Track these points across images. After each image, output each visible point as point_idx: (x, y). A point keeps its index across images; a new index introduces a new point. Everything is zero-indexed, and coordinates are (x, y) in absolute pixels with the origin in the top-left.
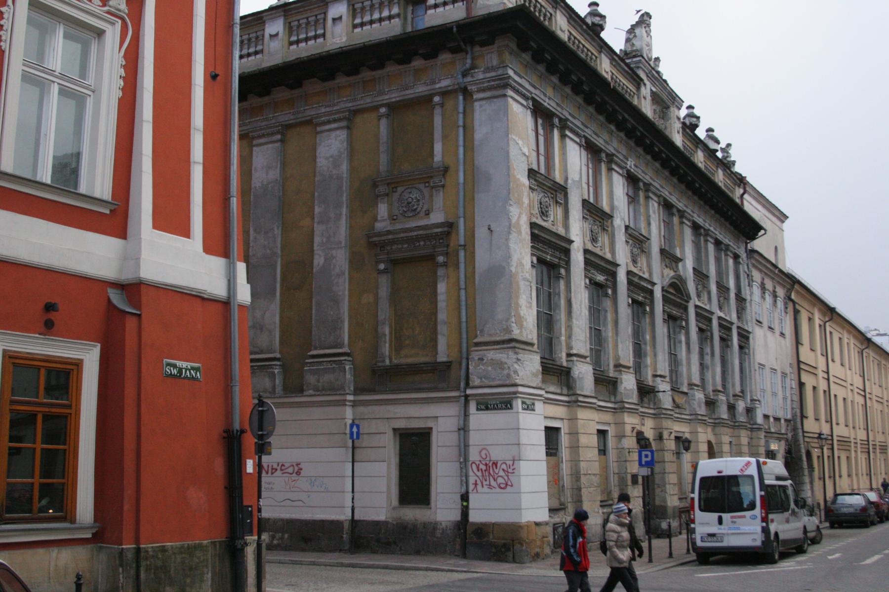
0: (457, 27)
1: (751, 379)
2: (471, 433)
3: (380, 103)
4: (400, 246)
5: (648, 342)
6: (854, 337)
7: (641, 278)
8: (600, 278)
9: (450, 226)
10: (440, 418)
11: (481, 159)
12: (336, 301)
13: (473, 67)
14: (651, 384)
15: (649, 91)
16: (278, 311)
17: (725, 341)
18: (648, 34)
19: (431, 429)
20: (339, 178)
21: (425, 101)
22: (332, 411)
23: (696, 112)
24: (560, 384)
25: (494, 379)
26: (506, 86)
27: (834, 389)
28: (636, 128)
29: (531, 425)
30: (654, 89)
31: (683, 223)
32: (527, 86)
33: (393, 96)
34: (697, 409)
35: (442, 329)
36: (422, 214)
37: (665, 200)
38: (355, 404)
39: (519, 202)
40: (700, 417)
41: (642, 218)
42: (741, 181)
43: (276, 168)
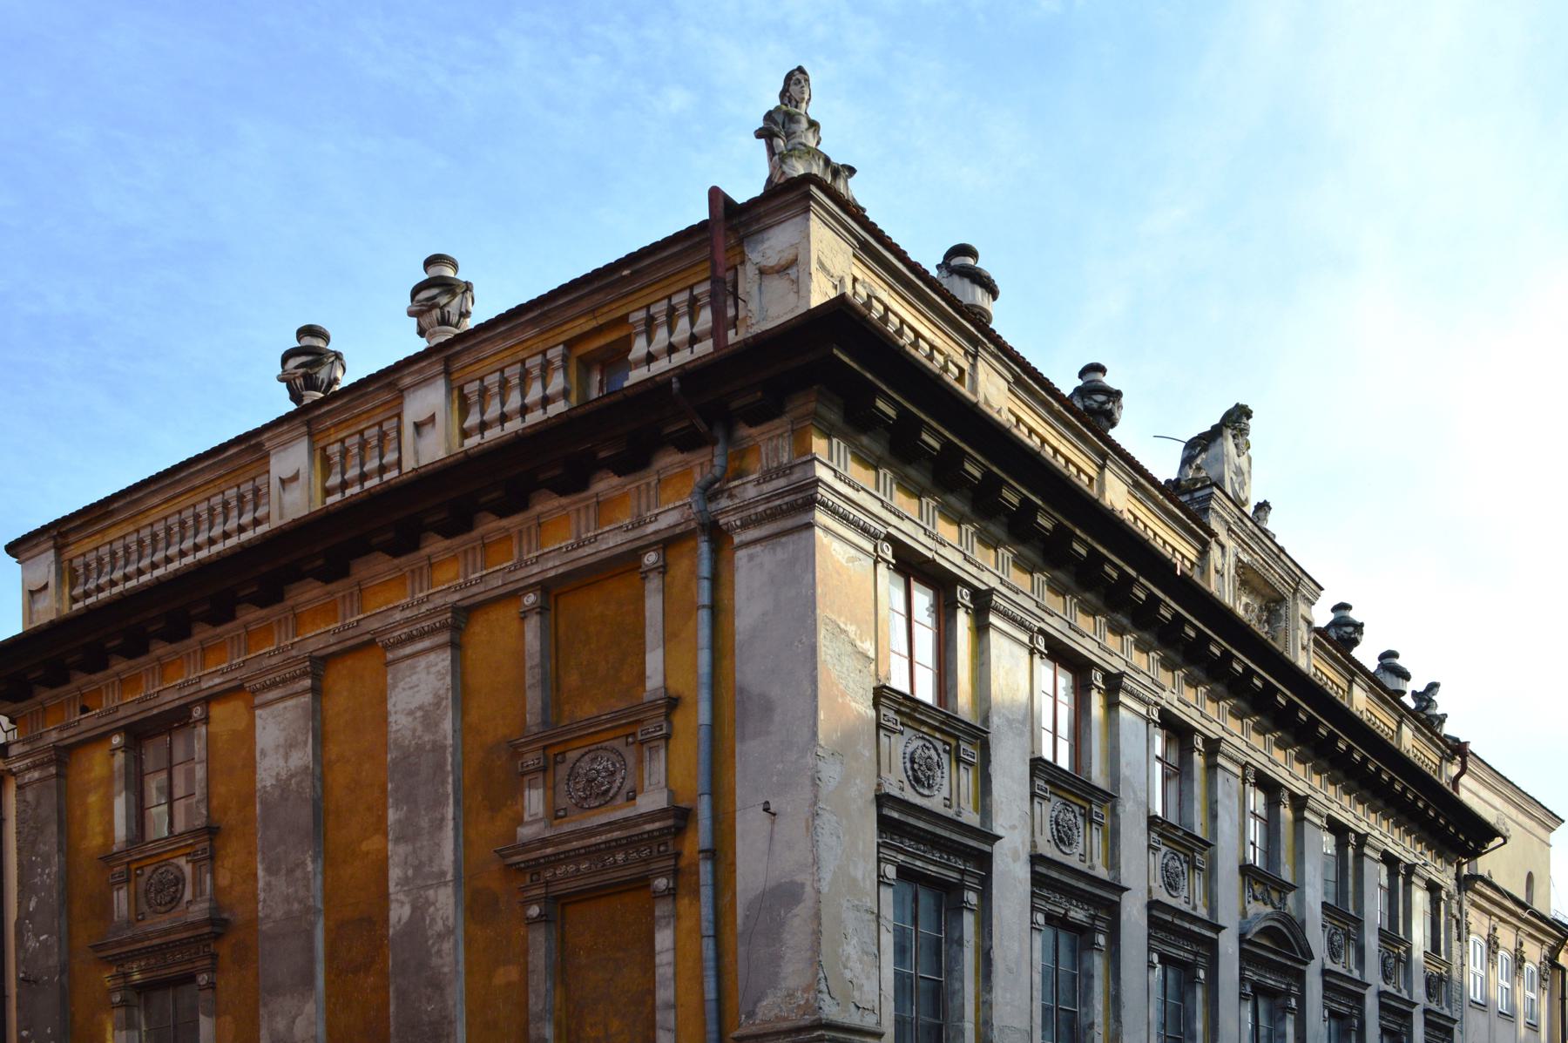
3: (521, 584)
4: (572, 868)
8: (1078, 915)
9: (681, 816)
11: (749, 671)
12: (437, 985)
15: (1232, 560)
18: (1243, 448)
20: (438, 748)
21: (625, 564)
23: (1354, 615)
28: (1133, 581)
30: (1245, 558)
32: (875, 507)
33: (550, 565)
36: (620, 800)
42: (1457, 750)
43: (306, 743)
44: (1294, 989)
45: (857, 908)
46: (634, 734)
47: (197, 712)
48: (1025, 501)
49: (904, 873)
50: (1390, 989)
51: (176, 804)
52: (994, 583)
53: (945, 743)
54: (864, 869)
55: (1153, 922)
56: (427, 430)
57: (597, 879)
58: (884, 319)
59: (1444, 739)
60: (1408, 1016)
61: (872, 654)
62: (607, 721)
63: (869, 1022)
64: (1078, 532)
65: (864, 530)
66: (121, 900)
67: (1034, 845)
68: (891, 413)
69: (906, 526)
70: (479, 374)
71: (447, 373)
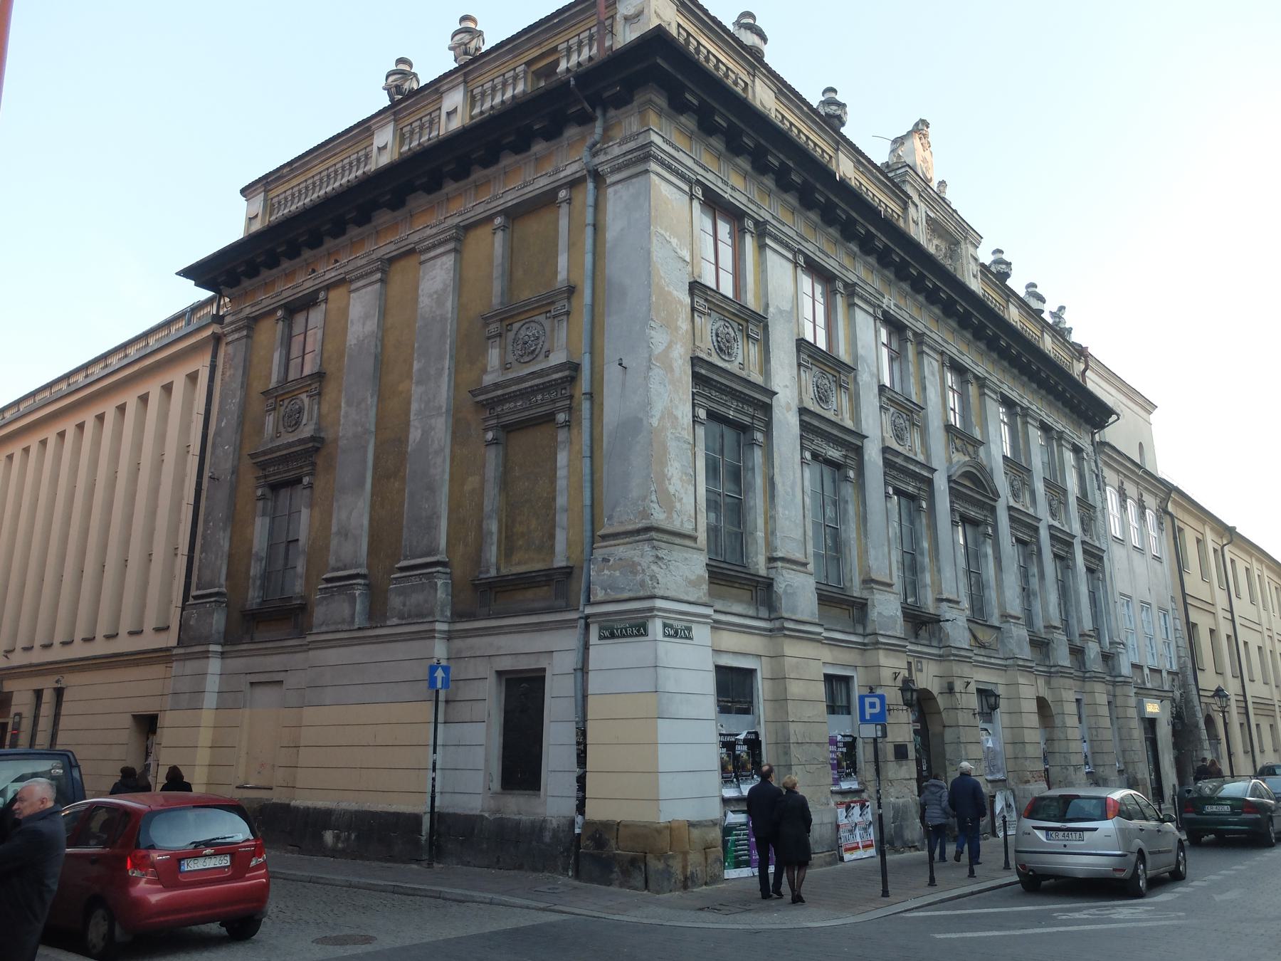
1: (1108, 613)
4: (512, 405)
5: (926, 553)
6: (1268, 567)
7: (907, 459)
8: (834, 453)
9: (575, 367)
10: (553, 650)
11: (614, 268)
12: (431, 488)
14: (932, 611)
16: (367, 509)
17: (1064, 559)
18: (927, 146)
19: (544, 670)
21: (547, 200)
22: (417, 647)
23: (1006, 257)
25: (623, 589)
26: (647, 157)
27: (1243, 635)
28: (874, 236)
30: (932, 215)
31: (923, 352)
32: (689, 163)
34: (1016, 651)
36: (541, 357)
37: (952, 360)
38: (450, 636)
39: (669, 325)
40: (1021, 663)
41: (912, 380)
42: (1081, 353)
44: (990, 520)
45: (678, 439)
48: (782, 163)
49: (711, 415)
50: (1056, 524)
51: (307, 357)
52: (768, 217)
54: (684, 412)
55: (888, 464)
56: (452, 117)
58: (698, 51)
59: (1073, 344)
60: (1070, 545)
64: (818, 186)
65: (682, 177)
66: (270, 420)
67: (801, 400)
68: (695, 102)
69: (710, 176)
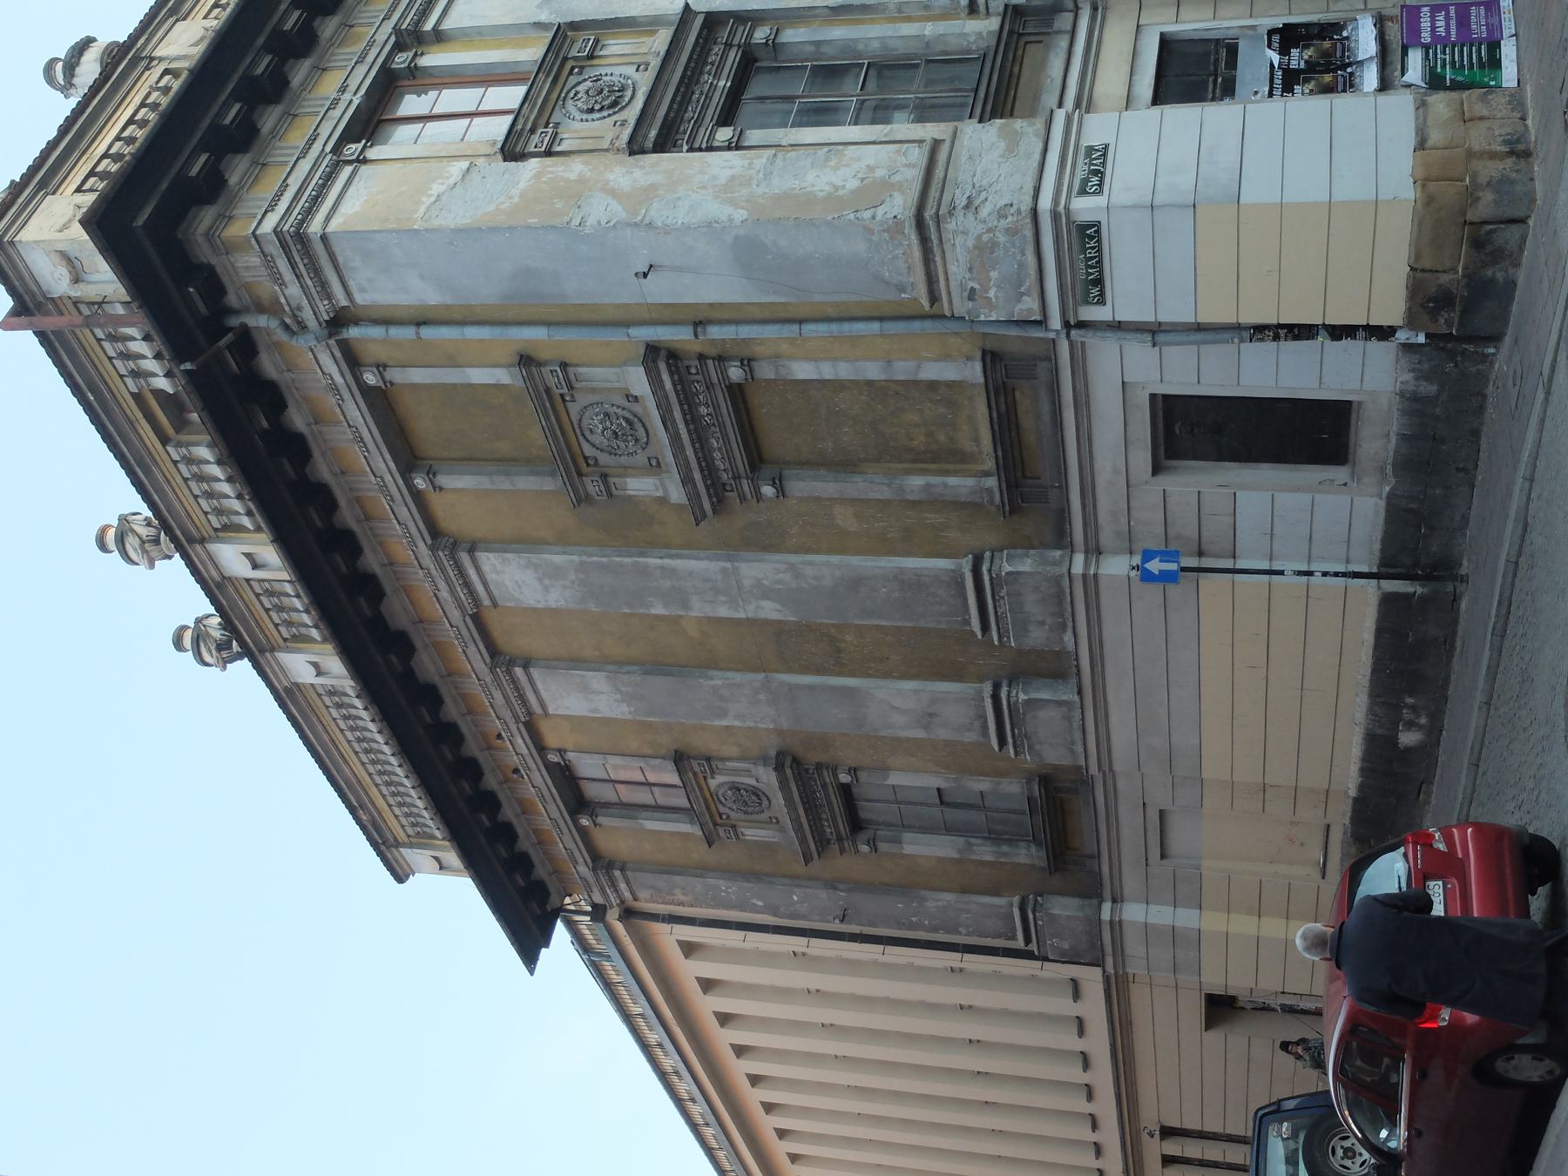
0: (183, 361)
2: (1161, 318)
3: (405, 491)
4: (717, 455)
9: (652, 353)
11: (485, 290)
12: (856, 583)
13: (273, 309)
19: (1153, 397)
21: (381, 403)
24: (1045, 34)
25: (1021, 265)
26: (301, 238)
29: (1152, 153)
32: (305, 166)
33: (383, 466)
35: (903, 370)
36: (637, 408)
38: (1095, 550)
39: (576, 194)
45: (768, 175)
46: (562, 396)
47: (554, 758)
52: (388, 27)
53: (571, 73)
54: (722, 165)
56: (259, 561)
57: (730, 431)
58: (117, 157)
61: (465, 164)
62: (547, 418)
63: (918, 156)
65: (329, 178)
67: (612, 149)
69: (325, 131)
70: (202, 517)
71: (202, 541)
